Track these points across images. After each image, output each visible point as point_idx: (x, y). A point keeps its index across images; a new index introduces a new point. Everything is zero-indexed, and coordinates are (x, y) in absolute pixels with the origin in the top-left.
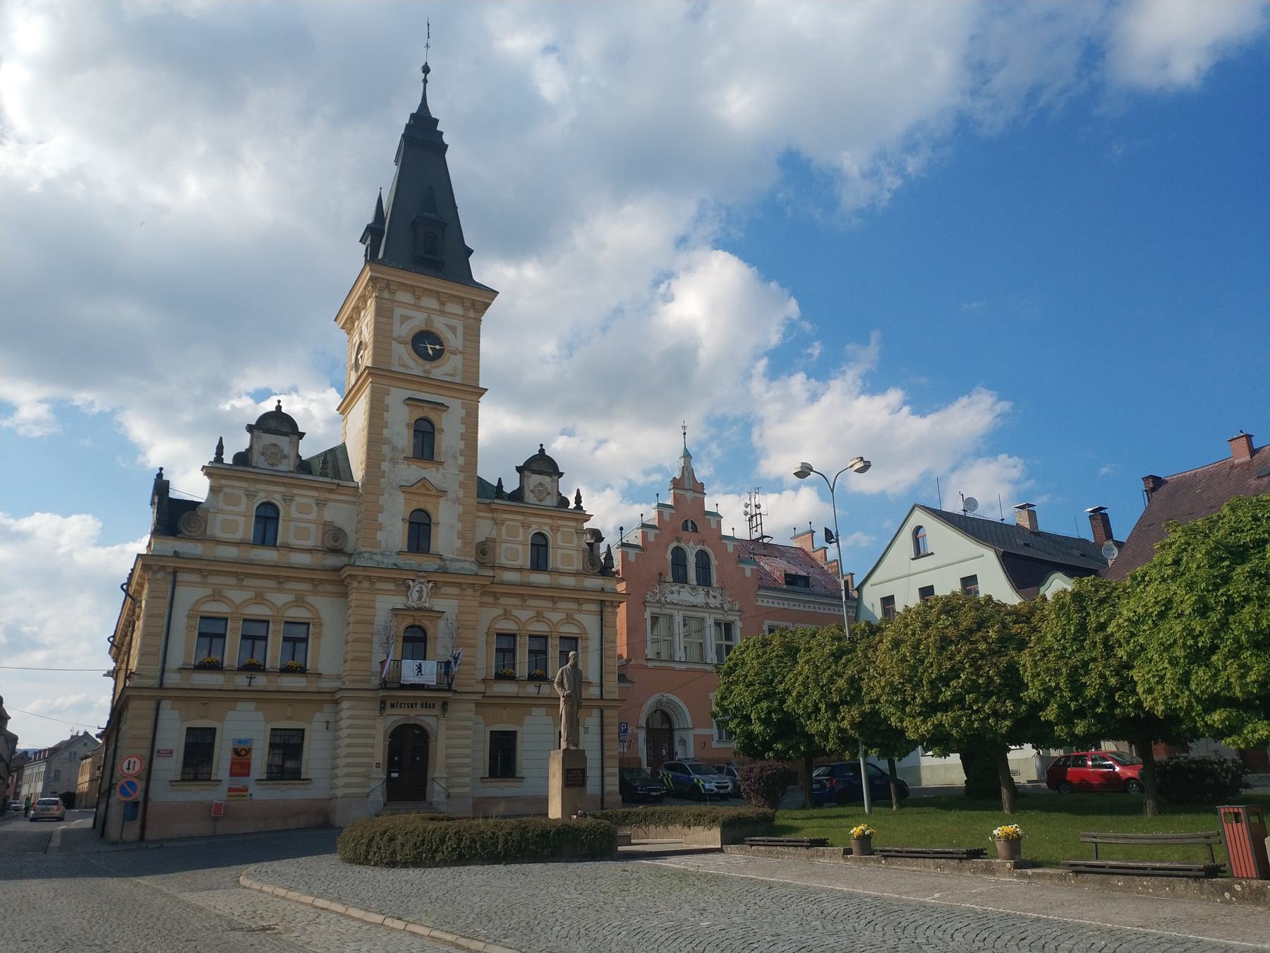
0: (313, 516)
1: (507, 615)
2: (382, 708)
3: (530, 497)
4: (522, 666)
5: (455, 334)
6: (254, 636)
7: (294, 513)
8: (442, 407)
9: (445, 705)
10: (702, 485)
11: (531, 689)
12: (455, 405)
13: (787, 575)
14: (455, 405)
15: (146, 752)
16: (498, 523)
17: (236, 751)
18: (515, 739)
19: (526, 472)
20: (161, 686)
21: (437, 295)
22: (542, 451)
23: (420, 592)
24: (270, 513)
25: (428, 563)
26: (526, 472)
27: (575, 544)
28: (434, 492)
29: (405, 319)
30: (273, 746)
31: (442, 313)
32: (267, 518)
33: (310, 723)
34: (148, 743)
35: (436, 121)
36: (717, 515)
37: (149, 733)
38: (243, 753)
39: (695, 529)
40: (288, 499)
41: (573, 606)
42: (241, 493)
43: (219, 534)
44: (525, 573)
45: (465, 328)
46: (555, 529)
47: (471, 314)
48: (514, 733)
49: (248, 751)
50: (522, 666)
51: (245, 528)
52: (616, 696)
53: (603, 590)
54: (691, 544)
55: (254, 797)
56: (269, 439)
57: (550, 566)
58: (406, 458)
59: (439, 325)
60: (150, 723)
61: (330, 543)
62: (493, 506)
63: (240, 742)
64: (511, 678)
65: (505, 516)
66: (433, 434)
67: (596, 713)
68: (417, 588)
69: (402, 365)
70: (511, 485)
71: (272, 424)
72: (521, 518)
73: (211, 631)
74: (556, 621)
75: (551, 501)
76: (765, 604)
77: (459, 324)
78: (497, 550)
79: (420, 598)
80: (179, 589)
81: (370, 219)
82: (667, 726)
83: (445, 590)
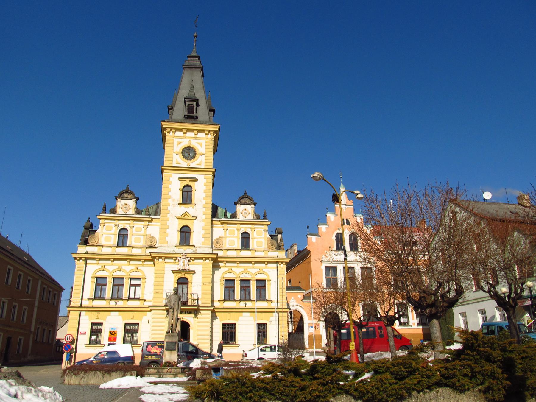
0: (142, 232)
5: (202, 146)
6: (245, 283)
8: (195, 180)
11: (242, 304)
16: (226, 230)
17: (111, 333)
18: (265, 328)
20: (81, 306)
23: (184, 262)
24: (125, 232)
29: (179, 143)
31: (196, 138)
33: (141, 320)
48: (235, 324)
49: (116, 332)
58: (179, 204)
61: (148, 244)
63: (112, 329)
64: (249, 300)
66: (191, 191)
69: (178, 163)
74: (253, 272)
77: (204, 142)
79: (184, 265)
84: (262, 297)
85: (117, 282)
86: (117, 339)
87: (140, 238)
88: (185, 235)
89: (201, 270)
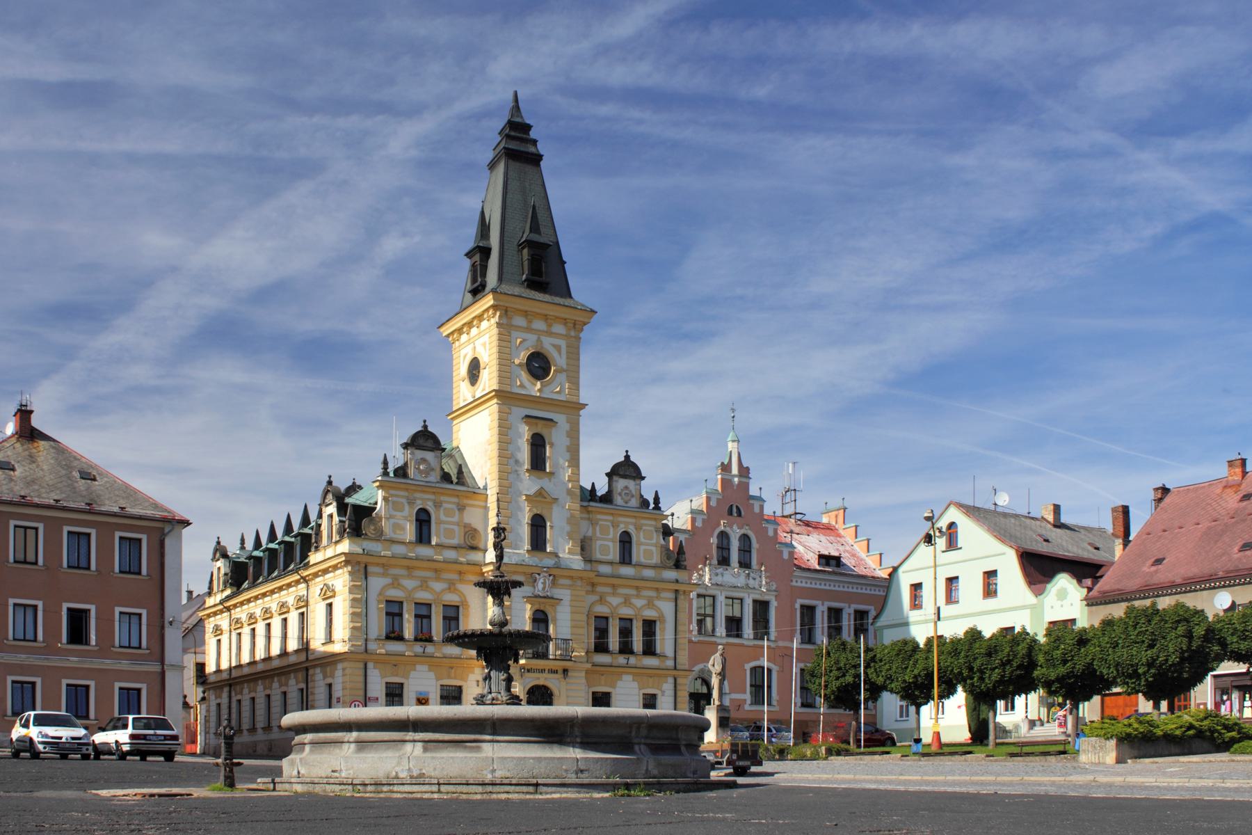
0: (455, 519)
1: (602, 600)
3: (618, 500)
4: (614, 641)
6: (423, 616)
9: (565, 671)
10: (748, 469)
11: (621, 660)
13: (821, 557)
14: (560, 418)
16: (593, 523)
19: (615, 478)
21: (545, 317)
22: (627, 457)
23: (544, 583)
26: (615, 478)
32: (423, 521)
34: (362, 693)
36: (760, 499)
39: (739, 514)
40: (438, 505)
42: (404, 501)
43: (598, 556)
47: (573, 333)
48: (460, 687)
50: (614, 641)
51: (614, 553)
52: (687, 667)
53: (677, 581)
54: (735, 527)
56: (420, 454)
57: (634, 559)
59: (548, 346)
65: (599, 517)
67: (671, 680)
70: (602, 489)
71: (421, 441)
73: (394, 612)
74: (638, 608)
75: (634, 502)
76: (799, 584)
77: (562, 343)
82: (705, 690)
83: (562, 581)
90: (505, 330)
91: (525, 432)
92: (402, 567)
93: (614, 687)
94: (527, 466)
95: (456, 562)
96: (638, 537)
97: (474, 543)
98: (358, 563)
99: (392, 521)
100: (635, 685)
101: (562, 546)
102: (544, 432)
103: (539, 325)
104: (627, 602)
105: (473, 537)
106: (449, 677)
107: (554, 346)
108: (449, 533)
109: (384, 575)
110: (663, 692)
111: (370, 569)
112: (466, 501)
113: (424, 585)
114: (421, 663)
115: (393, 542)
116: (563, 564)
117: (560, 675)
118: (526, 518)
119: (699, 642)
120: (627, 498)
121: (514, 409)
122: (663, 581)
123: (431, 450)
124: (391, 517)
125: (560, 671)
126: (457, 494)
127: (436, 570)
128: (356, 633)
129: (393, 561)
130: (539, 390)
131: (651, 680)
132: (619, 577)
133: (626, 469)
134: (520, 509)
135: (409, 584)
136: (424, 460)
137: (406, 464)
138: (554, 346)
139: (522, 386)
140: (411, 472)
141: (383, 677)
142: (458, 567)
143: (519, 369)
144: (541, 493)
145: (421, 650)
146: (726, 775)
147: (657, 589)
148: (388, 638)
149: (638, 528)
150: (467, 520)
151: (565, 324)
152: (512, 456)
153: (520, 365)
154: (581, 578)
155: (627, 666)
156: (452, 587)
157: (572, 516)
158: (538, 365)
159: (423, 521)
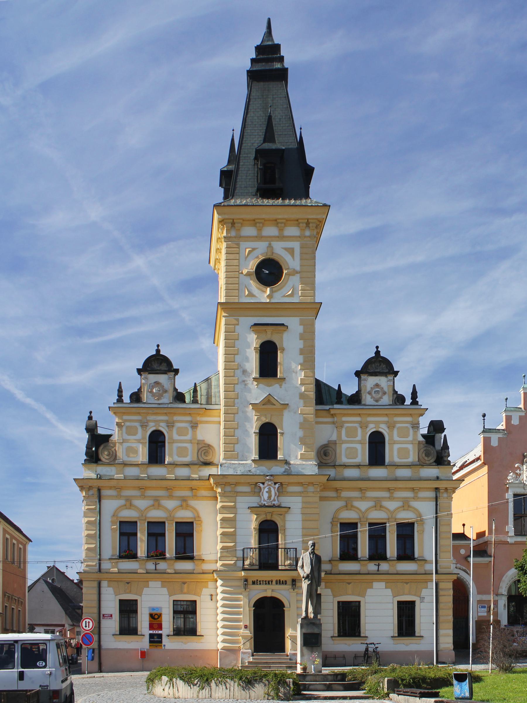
0: (189, 437)
1: (348, 505)
2: (246, 586)
3: (367, 399)
5: (293, 256)
6: (156, 531)
7: (176, 437)
11: (372, 566)
12: (294, 324)
14: (294, 324)
15: (96, 616)
16: (339, 426)
17: (151, 616)
19: (363, 377)
21: (276, 222)
22: (378, 353)
23: (269, 492)
25: (277, 469)
26: (363, 377)
27: (410, 438)
28: (278, 406)
30: (175, 612)
32: (157, 444)
34: (96, 610)
35: (253, 60)
37: (95, 604)
38: (156, 617)
40: (170, 425)
41: (410, 494)
42: (137, 424)
43: (344, 460)
44: (364, 469)
45: (302, 247)
46: (391, 426)
49: (160, 616)
51: (362, 454)
55: (167, 647)
56: (153, 378)
57: (387, 460)
59: (279, 250)
60: (96, 597)
62: (332, 412)
63: (153, 609)
64: (384, 558)
65: (344, 419)
68: (266, 490)
71: (155, 366)
72: (358, 419)
73: (127, 531)
74: (392, 511)
75: (386, 400)
77: (296, 245)
78: (338, 451)
79: (269, 497)
80: (103, 502)
81: (223, 162)
83: (291, 489)
84: (406, 553)
85: (156, 530)
86: (163, 626)
87: (356, 449)
88: (268, 438)
89: (300, 505)
90: (233, 242)
91: (253, 341)
92: (134, 488)
93: (364, 596)
94: (255, 374)
95: (189, 479)
96: (391, 436)
97: (208, 459)
98: (90, 488)
99: (126, 445)
100: (389, 592)
101: (295, 453)
102: (275, 339)
103: (271, 231)
104: (378, 505)
105: (206, 453)
106: (182, 592)
107: (286, 249)
108: (182, 452)
109: (118, 497)
110: (422, 599)
111: (104, 492)
112: (199, 418)
113: (157, 503)
114: (153, 579)
115: (125, 464)
116: (294, 470)
117: (288, 587)
118: (253, 428)
119: (516, 543)
120: (378, 396)
121: (241, 319)
122: (420, 479)
123: (165, 372)
124: (124, 441)
125: (289, 582)
126: (188, 412)
127: (167, 489)
128: (91, 554)
129: (148, 483)
130: (268, 296)
131: (407, 586)
132: (368, 479)
133: (379, 365)
134: (247, 419)
135: (141, 504)
136: (157, 383)
137: (140, 390)
138: (286, 249)
139: (251, 295)
140: (145, 396)
141: (334, 596)
142: (165, 483)
143: (248, 278)
144: (268, 401)
145: (376, 568)
146: (364, 693)
147: (413, 489)
148: (121, 557)
149: (391, 426)
150: (200, 437)
151: (298, 225)
152: (239, 366)
153: (248, 274)
154: (312, 484)
155: (378, 573)
156: (184, 502)
157: (305, 420)
158: (269, 272)
159: (157, 444)
